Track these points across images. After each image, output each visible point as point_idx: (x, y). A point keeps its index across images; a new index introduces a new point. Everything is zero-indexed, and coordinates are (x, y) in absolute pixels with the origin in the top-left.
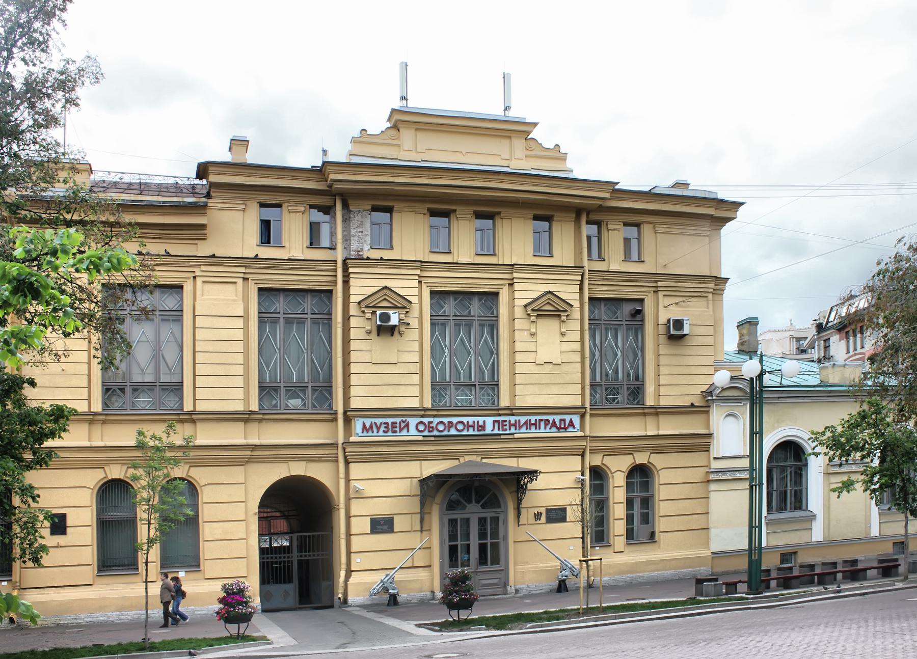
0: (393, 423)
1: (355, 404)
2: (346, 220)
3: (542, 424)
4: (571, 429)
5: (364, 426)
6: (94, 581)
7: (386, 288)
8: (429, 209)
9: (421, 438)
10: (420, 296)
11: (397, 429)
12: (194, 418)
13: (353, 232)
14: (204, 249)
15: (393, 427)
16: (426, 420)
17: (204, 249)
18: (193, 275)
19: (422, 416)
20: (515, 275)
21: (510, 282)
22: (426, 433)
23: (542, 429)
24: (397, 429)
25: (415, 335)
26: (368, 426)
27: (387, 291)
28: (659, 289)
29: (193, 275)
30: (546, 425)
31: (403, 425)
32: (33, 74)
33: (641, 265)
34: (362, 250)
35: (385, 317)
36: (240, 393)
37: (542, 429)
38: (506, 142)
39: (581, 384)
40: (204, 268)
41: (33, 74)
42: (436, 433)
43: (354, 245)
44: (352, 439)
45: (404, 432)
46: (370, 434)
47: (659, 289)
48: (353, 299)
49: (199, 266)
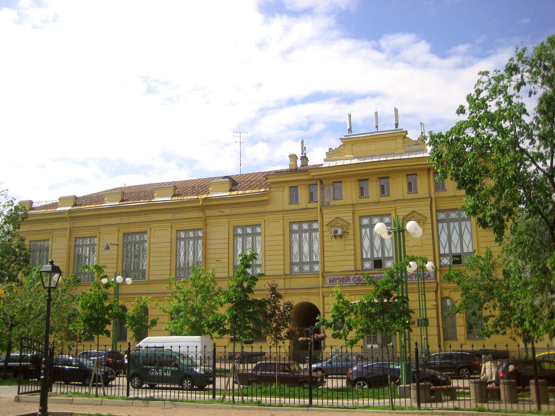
0: (343, 278)
1: (327, 270)
2: (322, 189)
3: (414, 276)
4: (429, 278)
5: (330, 281)
6: (465, 342)
7: (338, 217)
8: (357, 180)
9: (355, 285)
10: (354, 220)
11: (345, 281)
12: (150, 282)
13: (325, 194)
14: (269, 208)
15: (343, 280)
16: (357, 276)
17: (269, 208)
18: (264, 220)
19: (356, 274)
20: (397, 205)
21: (395, 208)
22: (358, 282)
23: (414, 279)
24: (345, 281)
25: (351, 237)
26: (332, 279)
27: (338, 219)
28: (397, 207)
29: (264, 220)
30: (416, 277)
31: (347, 279)
32: (532, 122)
33: (417, 194)
34: (330, 201)
35: (336, 232)
36: (282, 267)
37: (414, 279)
38: (394, 142)
39: (445, 254)
40: (268, 216)
41: (532, 122)
42: (362, 282)
43: (326, 200)
44: (325, 286)
45: (348, 282)
46: (333, 283)
47: (397, 207)
48: (325, 224)
49: (266, 216)
